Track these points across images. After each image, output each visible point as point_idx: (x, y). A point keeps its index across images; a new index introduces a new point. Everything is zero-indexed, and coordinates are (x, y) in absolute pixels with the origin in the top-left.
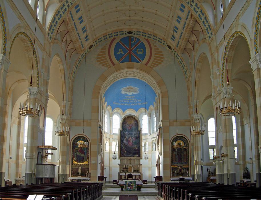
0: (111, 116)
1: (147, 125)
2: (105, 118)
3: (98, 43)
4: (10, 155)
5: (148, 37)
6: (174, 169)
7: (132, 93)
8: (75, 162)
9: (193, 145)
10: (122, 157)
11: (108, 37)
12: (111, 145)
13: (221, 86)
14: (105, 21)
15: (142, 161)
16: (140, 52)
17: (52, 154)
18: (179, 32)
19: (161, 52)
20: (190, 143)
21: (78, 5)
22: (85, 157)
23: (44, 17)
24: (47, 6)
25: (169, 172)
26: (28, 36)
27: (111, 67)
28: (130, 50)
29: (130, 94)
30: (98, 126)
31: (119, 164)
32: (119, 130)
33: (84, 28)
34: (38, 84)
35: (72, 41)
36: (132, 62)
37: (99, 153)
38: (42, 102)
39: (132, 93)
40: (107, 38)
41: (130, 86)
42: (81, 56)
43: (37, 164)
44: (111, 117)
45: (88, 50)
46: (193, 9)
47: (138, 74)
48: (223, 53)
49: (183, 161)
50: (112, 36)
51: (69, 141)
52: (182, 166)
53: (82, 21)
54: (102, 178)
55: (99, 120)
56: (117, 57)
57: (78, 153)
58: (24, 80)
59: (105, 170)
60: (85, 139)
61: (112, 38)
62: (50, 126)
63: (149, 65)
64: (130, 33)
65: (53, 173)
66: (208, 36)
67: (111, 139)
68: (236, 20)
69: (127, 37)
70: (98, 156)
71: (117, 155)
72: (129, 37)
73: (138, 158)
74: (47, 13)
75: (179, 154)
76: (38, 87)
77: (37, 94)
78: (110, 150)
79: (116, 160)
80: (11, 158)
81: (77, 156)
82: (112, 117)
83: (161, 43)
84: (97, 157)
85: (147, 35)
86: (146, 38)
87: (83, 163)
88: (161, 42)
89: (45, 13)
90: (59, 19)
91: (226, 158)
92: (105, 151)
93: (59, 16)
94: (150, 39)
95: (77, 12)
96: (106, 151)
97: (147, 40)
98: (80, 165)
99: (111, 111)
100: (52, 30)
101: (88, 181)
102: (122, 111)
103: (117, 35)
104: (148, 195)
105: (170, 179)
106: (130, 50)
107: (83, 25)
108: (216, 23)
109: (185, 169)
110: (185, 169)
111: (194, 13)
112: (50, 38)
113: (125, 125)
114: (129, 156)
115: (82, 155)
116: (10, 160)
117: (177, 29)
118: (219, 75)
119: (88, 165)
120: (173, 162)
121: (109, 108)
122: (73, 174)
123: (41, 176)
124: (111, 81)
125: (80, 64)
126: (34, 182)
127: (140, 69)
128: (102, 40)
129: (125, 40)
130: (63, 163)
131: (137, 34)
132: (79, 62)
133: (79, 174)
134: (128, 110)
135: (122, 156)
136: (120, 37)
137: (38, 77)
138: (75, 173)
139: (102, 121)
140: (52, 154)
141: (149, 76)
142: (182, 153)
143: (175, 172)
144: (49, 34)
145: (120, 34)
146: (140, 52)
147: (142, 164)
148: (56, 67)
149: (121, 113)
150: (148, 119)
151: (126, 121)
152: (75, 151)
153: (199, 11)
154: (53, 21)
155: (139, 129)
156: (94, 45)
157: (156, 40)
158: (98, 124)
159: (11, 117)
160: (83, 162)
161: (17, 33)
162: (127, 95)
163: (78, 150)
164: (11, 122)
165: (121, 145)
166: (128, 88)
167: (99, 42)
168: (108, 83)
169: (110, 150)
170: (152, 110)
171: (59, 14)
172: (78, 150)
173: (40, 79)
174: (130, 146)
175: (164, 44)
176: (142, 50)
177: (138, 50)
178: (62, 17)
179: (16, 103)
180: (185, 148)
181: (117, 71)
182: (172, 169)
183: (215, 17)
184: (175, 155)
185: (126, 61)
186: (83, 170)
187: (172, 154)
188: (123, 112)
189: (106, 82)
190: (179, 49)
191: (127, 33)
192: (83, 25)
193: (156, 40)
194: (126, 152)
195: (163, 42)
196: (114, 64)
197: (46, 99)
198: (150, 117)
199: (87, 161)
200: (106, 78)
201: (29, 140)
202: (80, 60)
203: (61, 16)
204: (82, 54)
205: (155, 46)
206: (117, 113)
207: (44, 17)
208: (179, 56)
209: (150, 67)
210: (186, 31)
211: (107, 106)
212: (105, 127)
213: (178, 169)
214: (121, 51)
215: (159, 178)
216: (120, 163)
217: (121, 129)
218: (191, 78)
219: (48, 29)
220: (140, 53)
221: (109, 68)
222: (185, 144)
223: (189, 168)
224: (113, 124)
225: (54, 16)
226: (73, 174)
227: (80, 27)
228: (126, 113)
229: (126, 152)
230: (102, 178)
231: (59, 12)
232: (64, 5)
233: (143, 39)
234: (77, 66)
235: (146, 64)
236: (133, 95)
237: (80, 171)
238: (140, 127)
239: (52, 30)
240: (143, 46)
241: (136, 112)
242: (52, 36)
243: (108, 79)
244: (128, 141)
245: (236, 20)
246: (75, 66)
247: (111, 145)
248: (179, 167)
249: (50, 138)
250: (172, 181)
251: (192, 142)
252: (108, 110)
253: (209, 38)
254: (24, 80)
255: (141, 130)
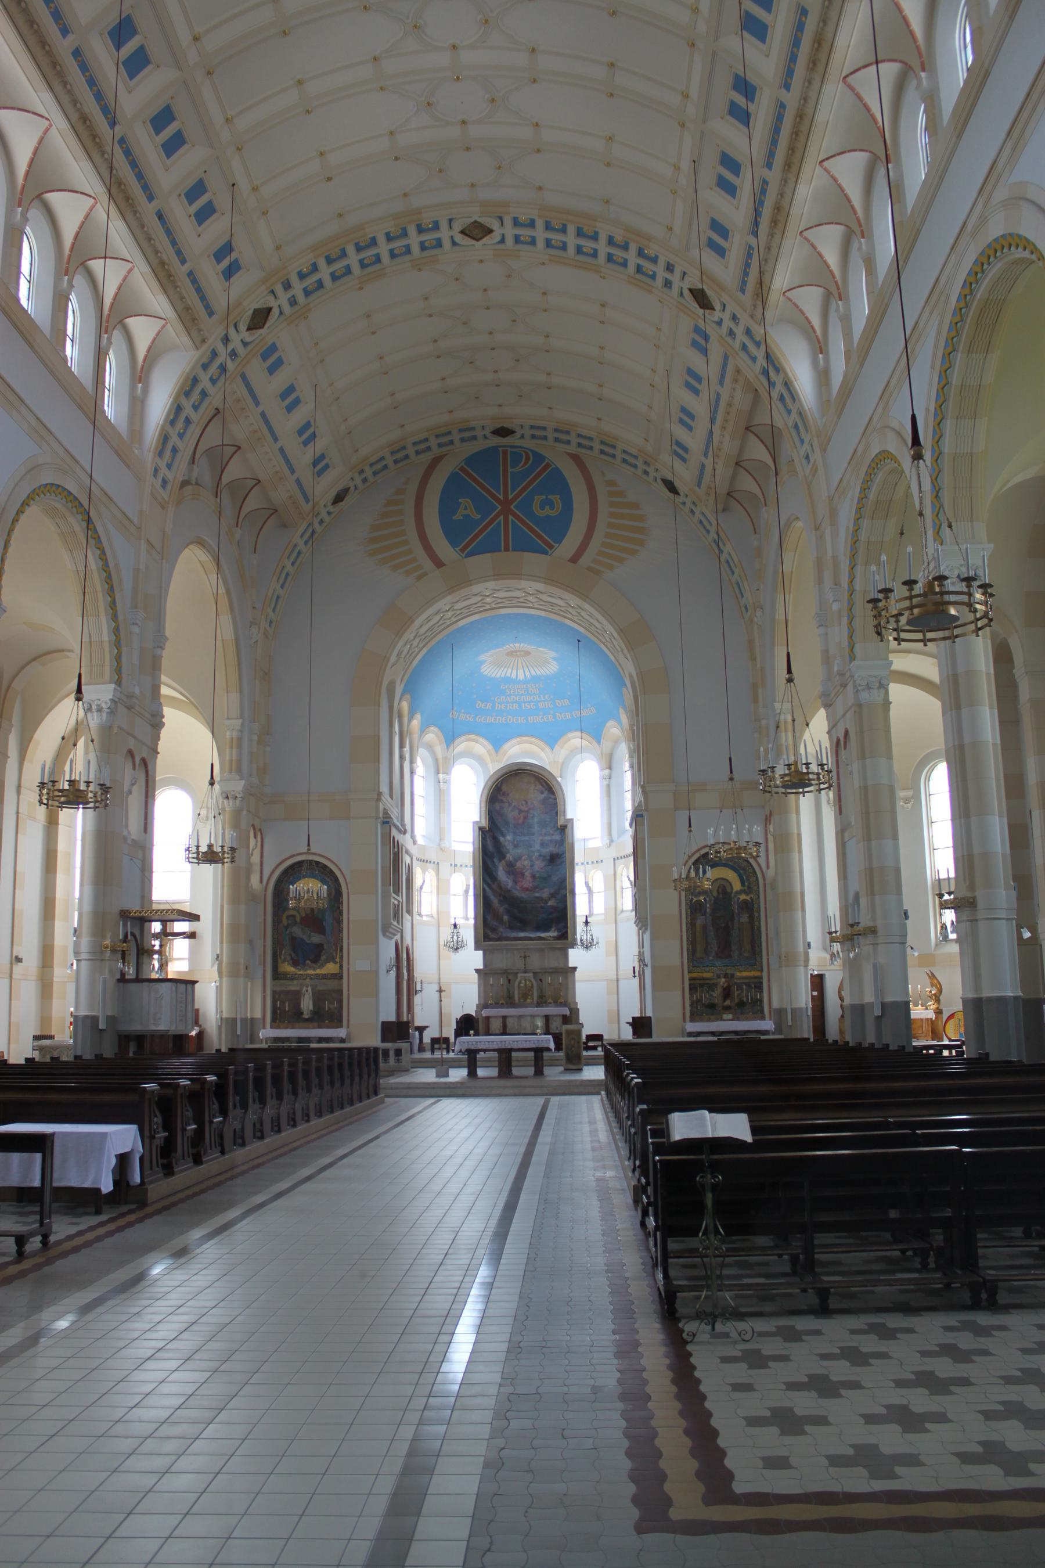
0: (440, 768)
1: (597, 804)
2: (416, 778)
3: (371, 478)
4: (15, 947)
5: (580, 445)
6: (702, 986)
7: (527, 671)
8: (288, 968)
9: (773, 887)
10: (490, 940)
11: (412, 455)
12: (442, 888)
13: (847, 656)
14: (393, 395)
15: (575, 956)
16: (547, 507)
17: (192, 935)
18: (702, 426)
19: (635, 506)
20: (764, 880)
21: (274, 344)
22: (325, 946)
23: (137, 405)
24: (144, 361)
25: (677, 1000)
26: (71, 493)
27: (425, 574)
28: (506, 503)
29: (521, 677)
30: (377, 818)
31: (477, 971)
32: (477, 830)
33: (308, 425)
34: (118, 670)
35: (259, 481)
36: (514, 550)
37: (387, 930)
38: (134, 737)
39: (527, 671)
40: (407, 457)
41: (517, 645)
42: (302, 536)
43: (119, 981)
44: (441, 776)
45: (331, 508)
46: (737, 345)
47: (544, 597)
48: (848, 527)
49: (737, 953)
50: (429, 449)
51: (261, 882)
52: (732, 976)
53: (297, 401)
54: (398, 1030)
55: (380, 794)
56: (454, 532)
57: (297, 931)
58: (62, 651)
59: (417, 999)
60: (323, 871)
61: (428, 457)
62: (177, 821)
63: (586, 560)
64: (503, 432)
65: (186, 1015)
66: (802, 452)
67: (445, 867)
68: (881, 406)
69: (494, 450)
70: (382, 940)
71: (468, 935)
72: (500, 449)
73: (559, 943)
74: (146, 391)
75: (718, 919)
76: (119, 683)
77: (112, 712)
78: (442, 913)
79: (462, 952)
80: (19, 960)
81: (296, 944)
82: (447, 772)
83: (633, 469)
84: (376, 943)
85: (574, 440)
86: (573, 449)
87: (318, 971)
88: (635, 466)
89: (139, 391)
90: (196, 408)
91: (870, 939)
92: (416, 917)
93: (196, 395)
94: (588, 452)
95: (272, 370)
96: (420, 915)
97: (576, 458)
98: (310, 977)
99: (439, 750)
100: (168, 453)
101: (343, 1041)
102: (490, 747)
103: (451, 442)
104: (506, 1095)
105: (683, 1029)
106: (506, 503)
107: (300, 416)
108: (824, 402)
109: (748, 985)
110: (748, 985)
111: (741, 360)
112: (164, 483)
113: (502, 808)
114: (522, 935)
115: (316, 939)
116: (18, 968)
117: (692, 417)
118: (840, 611)
119: (341, 978)
120: (695, 955)
121: (432, 736)
122: (279, 1017)
123: (136, 1027)
124: (431, 629)
125: (296, 566)
126: (109, 1051)
127: (548, 580)
128: (386, 467)
129: (484, 462)
130: (235, 971)
131: (533, 437)
132: (292, 559)
133: (306, 1016)
134: (515, 741)
135: (493, 936)
136: (464, 451)
137: (118, 644)
138: (285, 1011)
139: (400, 796)
140: (192, 935)
141: (586, 606)
142: (732, 919)
143: (703, 1001)
144: (156, 471)
145: (463, 440)
146: (547, 507)
147: (575, 969)
148: (193, 586)
149: (487, 758)
150: (603, 778)
151: (504, 788)
152: (285, 922)
153: (760, 354)
154: (172, 417)
155: (560, 822)
156: (356, 488)
157: (614, 456)
158: (377, 808)
159: (19, 792)
160: (321, 967)
161: (28, 491)
162: (507, 680)
163: (298, 919)
164: (18, 813)
165: (484, 890)
166: (511, 654)
167: (375, 474)
168: (417, 640)
169: (442, 913)
170: (616, 742)
171: (182, 418)
172: (298, 919)
173: (124, 650)
174: (524, 895)
175: (646, 473)
176: (556, 498)
177: (538, 499)
178: (207, 401)
179: (36, 736)
180: (743, 897)
181: (452, 589)
182: (693, 988)
183: (823, 376)
184: (704, 927)
185: (490, 547)
186: (319, 998)
187: (692, 925)
188: (493, 752)
189: (409, 635)
190: (708, 494)
191: (489, 435)
192: (300, 416)
193: (614, 456)
194: (506, 918)
195: (641, 466)
196: (439, 563)
197: (152, 726)
198: (610, 768)
199: (336, 963)
200: (411, 620)
201: (88, 889)
202: (299, 553)
203: (204, 394)
204: (304, 525)
205: (611, 483)
206: (468, 754)
207: (137, 405)
208: (711, 524)
209: (589, 569)
210: (724, 428)
211: (423, 731)
212: (417, 819)
213: (716, 985)
214: (466, 508)
215: (641, 1025)
216: (481, 967)
217: (485, 823)
218: (759, 613)
219: (151, 454)
220: (547, 511)
221: (420, 577)
222: (743, 884)
223: (761, 983)
224: (443, 810)
225: (176, 399)
226: (279, 1017)
227: (288, 425)
228: (506, 757)
229: (506, 918)
230: (398, 1030)
231: (195, 381)
232: (214, 354)
233: (558, 458)
234: (287, 574)
235: (574, 560)
236: (535, 679)
237: (307, 1004)
238: (565, 815)
239: (168, 453)
240: (557, 483)
241: (548, 749)
242: (170, 476)
243: (417, 623)
244: (512, 869)
245: (881, 406)
246: (275, 578)
247: (442, 888)
248: (719, 977)
249: (174, 878)
250: (690, 1034)
251: (770, 873)
252: (430, 748)
253: (804, 461)
254: (62, 651)
255: (569, 827)
